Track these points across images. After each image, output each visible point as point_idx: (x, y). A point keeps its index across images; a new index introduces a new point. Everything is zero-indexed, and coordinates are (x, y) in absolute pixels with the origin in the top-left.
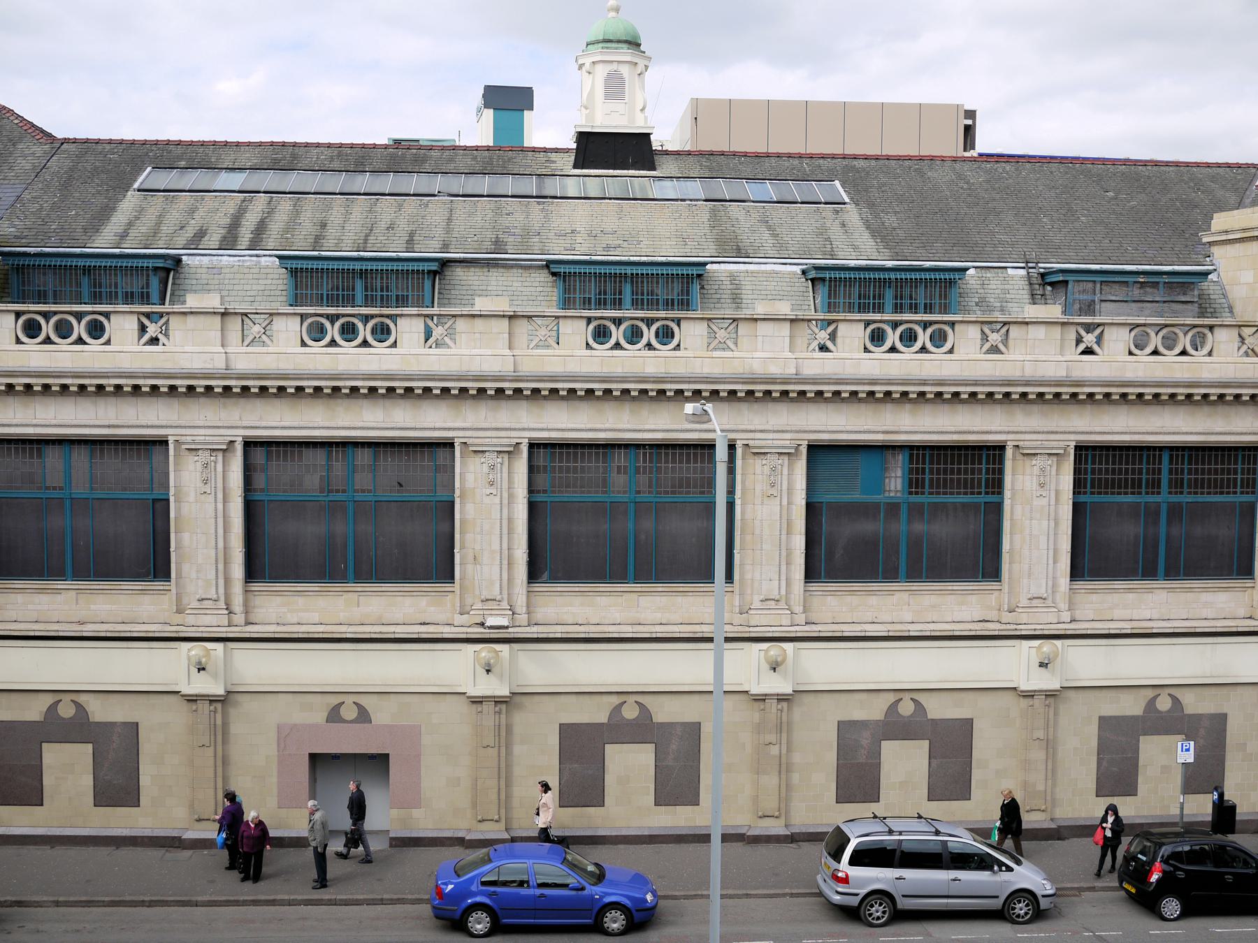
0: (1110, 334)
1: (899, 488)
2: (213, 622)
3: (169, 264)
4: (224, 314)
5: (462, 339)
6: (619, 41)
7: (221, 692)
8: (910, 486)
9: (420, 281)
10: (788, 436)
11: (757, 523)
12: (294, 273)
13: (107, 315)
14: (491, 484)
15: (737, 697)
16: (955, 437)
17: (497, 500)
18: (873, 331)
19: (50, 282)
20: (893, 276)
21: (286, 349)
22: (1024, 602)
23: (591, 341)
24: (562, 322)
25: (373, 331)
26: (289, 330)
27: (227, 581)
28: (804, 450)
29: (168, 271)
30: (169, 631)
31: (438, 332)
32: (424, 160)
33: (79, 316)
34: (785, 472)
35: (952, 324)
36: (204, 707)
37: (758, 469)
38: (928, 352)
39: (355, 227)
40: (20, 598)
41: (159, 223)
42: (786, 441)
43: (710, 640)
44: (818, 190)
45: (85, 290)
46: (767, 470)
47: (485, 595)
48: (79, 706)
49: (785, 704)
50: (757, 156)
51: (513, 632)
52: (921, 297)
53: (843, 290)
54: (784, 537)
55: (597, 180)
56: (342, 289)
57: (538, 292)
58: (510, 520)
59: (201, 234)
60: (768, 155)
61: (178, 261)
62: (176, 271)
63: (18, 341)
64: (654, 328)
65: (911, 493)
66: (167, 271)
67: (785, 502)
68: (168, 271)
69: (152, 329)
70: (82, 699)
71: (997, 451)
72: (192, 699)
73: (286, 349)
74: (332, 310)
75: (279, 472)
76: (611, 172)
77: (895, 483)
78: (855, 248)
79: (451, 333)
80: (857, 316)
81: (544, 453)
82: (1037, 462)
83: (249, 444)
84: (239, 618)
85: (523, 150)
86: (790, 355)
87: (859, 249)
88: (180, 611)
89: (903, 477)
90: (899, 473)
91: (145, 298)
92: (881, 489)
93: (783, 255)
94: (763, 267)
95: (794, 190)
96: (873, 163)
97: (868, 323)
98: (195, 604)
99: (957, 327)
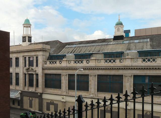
0: (72, 61)
1: (148, 81)
2: (65, 94)
3: (122, 52)
4: (66, 61)
5: (124, 62)
6: (119, 24)
7: (65, 101)
8: (149, 81)
9: (87, 56)
10: (131, 74)
11: (126, 86)
12: (75, 56)
13: (83, 60)
14: (93, 80)
15: (123, 109)
16: (156, 74)
17: (93, 81)
18: (148, 59)
19: (54, 58)
20: (149, 52)
21: (103, 64)
22: (63, 92)
23: (105, 62)
24: (138, 59)
25: (148, 60)
26: (103, 61)
27: (66, 89)
28: (133, 76)
29: (122, 53)
30: (60, 94)
31: (121, 61)
32: (106, 41)
33: (54, 61)
34: (130, 79)
35: (156, 58)
36: (63, 103)
37: (126, 78)
38: (147, 62)
39: (85, 50)
40: (49, 90)
41: (65, 52)
42: (130, 75)
43: (75, 97)
44: (145, 40)
45: (112, 57)
46: (127, 79)
47: (92, 93)
48: (53, 101)
49: (129, 111)
50: (139, 36)
51: (94, 98)
52: (54, 58)
53: (143, 54)
54: (130, 88)
55: (116, 42)
56: (80, 57)
57: (101, 57)
58: (95, 84)
59: (69, 52)
60: (140, 36)
61: (66, 55)
62: (123, 53)
63: (105, 63)
64: (113, 60)
65: (149, 82)
66: (64, 56)
67: (130, 83)
68: (122, 53)
69: (88, 62)
70: (53, 101)
71: (60, 75)
72: (62, 102)
73: (103, 64)
74: (80, 60)
75: (48, 77)
76: (120, 40)
77: (147, 81)
78: (147, 48)
79: (123, 61)
80: (141, 58)
81: (135, 77)
82: (64, 76)
83: (69, 75)
84: (67, 93)
85: (129, 37)
86: (130, 63)
87: (148, 48)
88: (62, 92)
89: (148, 80)
90: (148, 79)
91: (120, 57)
92: (145, 81)
93: (135, 49)
94: (132, 52)
95: (142, 41)
96: (156, 35)
97: (142, 58)
98: (63, 92)
99: (157, 58)
